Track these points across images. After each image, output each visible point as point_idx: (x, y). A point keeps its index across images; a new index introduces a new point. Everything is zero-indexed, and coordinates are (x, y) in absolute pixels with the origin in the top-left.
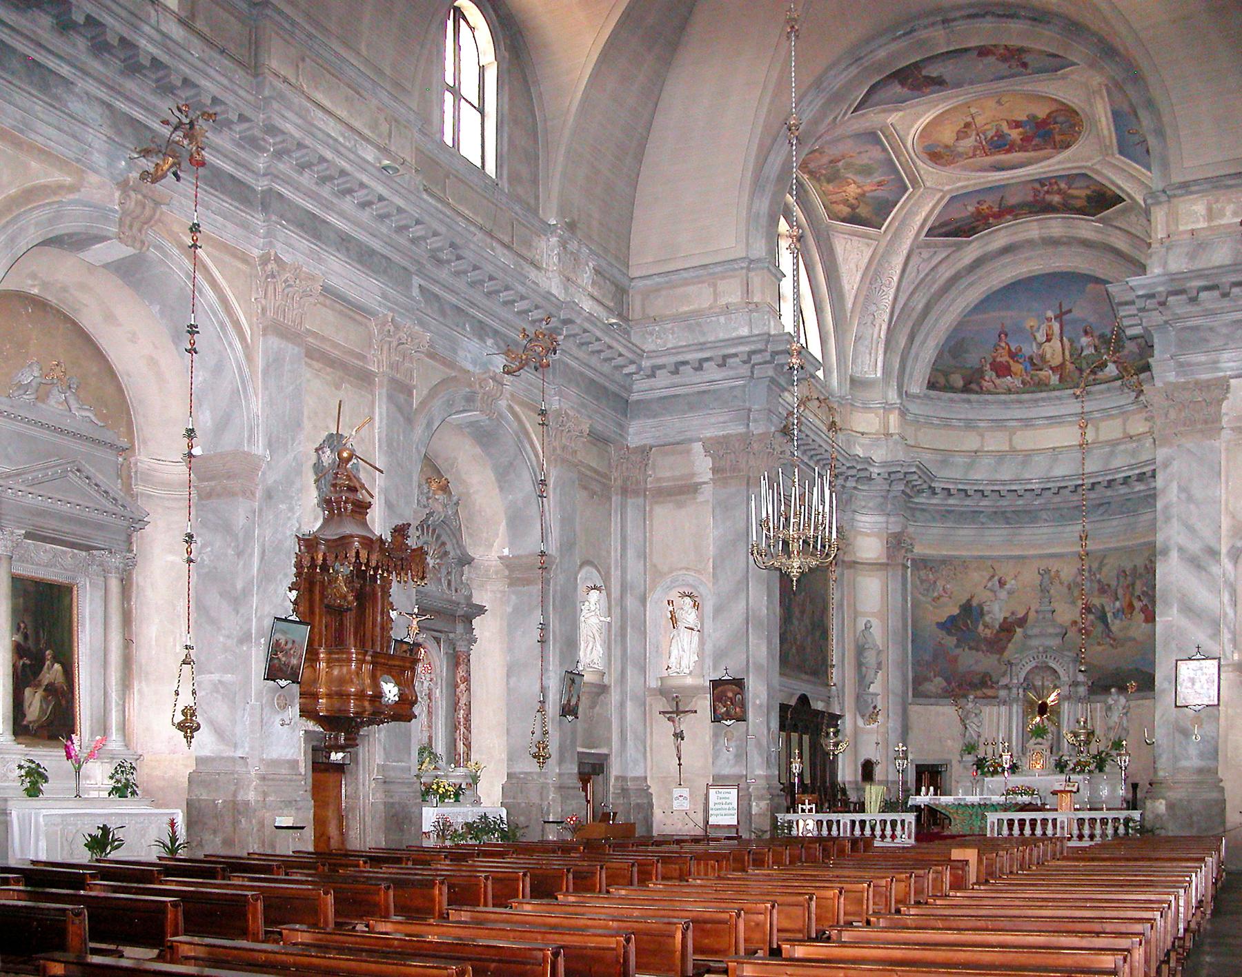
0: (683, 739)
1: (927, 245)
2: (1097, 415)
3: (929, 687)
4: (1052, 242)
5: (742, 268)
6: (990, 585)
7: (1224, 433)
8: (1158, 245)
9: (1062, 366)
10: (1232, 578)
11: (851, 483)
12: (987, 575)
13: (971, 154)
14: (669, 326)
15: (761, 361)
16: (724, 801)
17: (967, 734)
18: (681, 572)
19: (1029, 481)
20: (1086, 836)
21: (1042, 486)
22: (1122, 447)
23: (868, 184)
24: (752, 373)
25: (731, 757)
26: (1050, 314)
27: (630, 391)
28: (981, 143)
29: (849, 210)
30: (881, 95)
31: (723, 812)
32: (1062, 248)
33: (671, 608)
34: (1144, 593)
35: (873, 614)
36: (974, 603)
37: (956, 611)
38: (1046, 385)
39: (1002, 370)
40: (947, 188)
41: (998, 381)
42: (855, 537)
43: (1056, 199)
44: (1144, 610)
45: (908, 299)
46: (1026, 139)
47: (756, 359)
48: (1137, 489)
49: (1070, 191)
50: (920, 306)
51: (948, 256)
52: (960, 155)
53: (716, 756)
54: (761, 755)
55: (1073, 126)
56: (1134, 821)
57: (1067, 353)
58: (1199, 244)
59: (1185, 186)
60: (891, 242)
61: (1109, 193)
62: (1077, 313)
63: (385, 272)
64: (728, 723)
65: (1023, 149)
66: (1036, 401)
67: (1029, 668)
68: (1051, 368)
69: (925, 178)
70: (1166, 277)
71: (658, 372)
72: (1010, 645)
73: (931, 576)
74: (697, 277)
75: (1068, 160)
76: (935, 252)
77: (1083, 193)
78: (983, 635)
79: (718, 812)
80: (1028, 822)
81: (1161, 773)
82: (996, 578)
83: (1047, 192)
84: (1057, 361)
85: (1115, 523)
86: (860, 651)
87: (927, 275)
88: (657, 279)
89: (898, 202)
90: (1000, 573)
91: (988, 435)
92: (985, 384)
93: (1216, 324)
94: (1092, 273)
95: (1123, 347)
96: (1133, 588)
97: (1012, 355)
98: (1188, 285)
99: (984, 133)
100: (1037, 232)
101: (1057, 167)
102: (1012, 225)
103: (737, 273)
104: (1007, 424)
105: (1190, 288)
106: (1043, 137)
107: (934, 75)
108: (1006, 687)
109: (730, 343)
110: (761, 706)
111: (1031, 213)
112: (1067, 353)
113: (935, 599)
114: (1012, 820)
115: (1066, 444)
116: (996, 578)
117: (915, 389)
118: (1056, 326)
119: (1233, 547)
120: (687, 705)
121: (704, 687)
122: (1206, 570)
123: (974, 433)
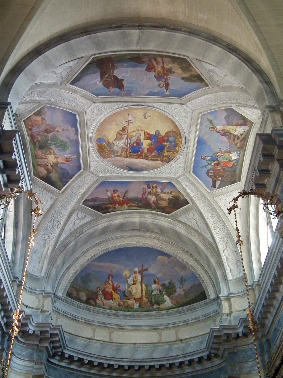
1: (82, 210)
9: (141, 299)
13: (119, 154)
19: (121, 360)
22: (176, 346)
26: (136, 269)
28: (127, 146)
29: (46, 172)
38: (132, 308)
39: (108, 296)
40: (101, 175)
41: (105, 302)
43: (153, 198)
48: (187, 371)
49: (162, 195)
52: (114, 152)
55: (176, 145)
61: (182, 198)
62: (151, 271)
65: (146, 158)
66: (126, 316)
68: (135, 299)
77: (166, 197)
84: (138, 296)
89: (73, 176)
91: (97, 330)
92: (98, 302)
94: (162, 250)
95: (175, 291)
97: (115, 289)
100: (138, 219)
107: (120, 77)
111: (139, 207)
117: (60, 294)
118: (139, 277)
123: (90, 328)
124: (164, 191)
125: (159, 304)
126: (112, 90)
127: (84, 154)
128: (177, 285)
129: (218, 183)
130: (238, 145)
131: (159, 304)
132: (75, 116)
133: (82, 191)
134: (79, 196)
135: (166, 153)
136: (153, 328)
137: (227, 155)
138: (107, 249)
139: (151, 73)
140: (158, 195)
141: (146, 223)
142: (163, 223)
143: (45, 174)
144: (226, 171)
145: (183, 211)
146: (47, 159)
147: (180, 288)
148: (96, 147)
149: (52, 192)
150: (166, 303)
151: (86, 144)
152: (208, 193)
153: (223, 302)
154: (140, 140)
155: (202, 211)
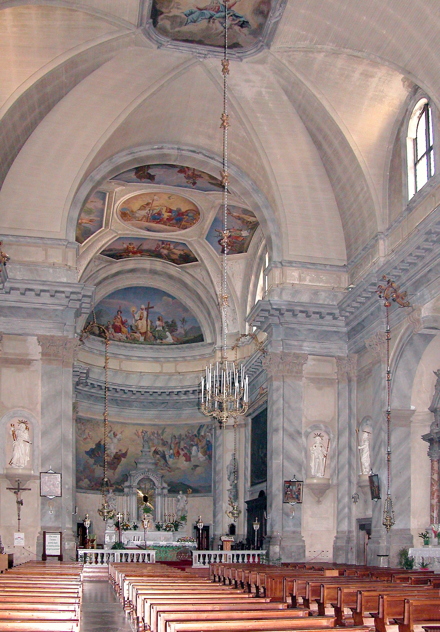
0: (22, 505)
1: (99, 259)
2: (162, 359)
4: (153, 272)
5: (64, 245)
6: (109, 435)
7: (304, 379)
8: (276, 287)
9: (145, 333)
15: (76, 299)
16: (53, 541)
19: (131, 386)
21: (137, 390)
22: (175, 377)
25: (52, 517)
26: (143, 307)
30: (125, 176)
31: (53, 548)
32: (156, 276)
33: (12, 429)
34: (185, 447)
36: (102, 443)
37: (94, 447)
38: (138, 341)
39: (118, 330)
40: (120, 232)
41: (115, 334)
43: (165, 252)
44: (185, 455)
47: (73, 297)
49: (174, 250)
51: (105, 267)
52: (135, 218)
53: (43, 515)
59: (290, 262)
62: (156, 309)
65: (165, 224)
68: (141, 333)
69: (112, 224)
70: (286, 303)
73: (83, 427)
74: (34, 243)
75: (182, 235)
76: (101, 263)
77: (178, 252)
79: (50, 548)
81: (275, 533)
82: (112, 432)
84: (144, 330)
85: (170, 412)
87: (94, 274)
88: (11, 238)
89: (95, 232)
90: (114, 430)
93: (301, 329)
97: (123, 323)
99: (153, 211)
100: (149, 266)
101: (175, 237)
102: (139, 259)
104: (118, 356)
106: (177, 220)
107: (152, 174)
109: (61, 284)
110: (68, 489)
113: (85, 439)
114: (97, 554)
115: (146, 371)
116: (112, 432)
118: (145, 313)
120: (23, 486)
122: (296, 441)
124: (176, 248)
125: (162, 340)
126: (143, 180)
127: (107, 217)
128: (179, 324)
130: (250, 227)
131: (162, 340)
132: (105, 194)
133: (100, 244)
134: (98, 248)
135: (183, 223)
136: (156, 360)
137: (238, 232)
138: (117, 288)
140: (171, 250)
141: (156, 270)
144: (236, 243)
145: (191, 265)
147: (181, 328)
150: (168, 339)
151: (111, 211)
152: (217, 257)
153: (217, 351)
154: (161, 212)
155: (210, 271)
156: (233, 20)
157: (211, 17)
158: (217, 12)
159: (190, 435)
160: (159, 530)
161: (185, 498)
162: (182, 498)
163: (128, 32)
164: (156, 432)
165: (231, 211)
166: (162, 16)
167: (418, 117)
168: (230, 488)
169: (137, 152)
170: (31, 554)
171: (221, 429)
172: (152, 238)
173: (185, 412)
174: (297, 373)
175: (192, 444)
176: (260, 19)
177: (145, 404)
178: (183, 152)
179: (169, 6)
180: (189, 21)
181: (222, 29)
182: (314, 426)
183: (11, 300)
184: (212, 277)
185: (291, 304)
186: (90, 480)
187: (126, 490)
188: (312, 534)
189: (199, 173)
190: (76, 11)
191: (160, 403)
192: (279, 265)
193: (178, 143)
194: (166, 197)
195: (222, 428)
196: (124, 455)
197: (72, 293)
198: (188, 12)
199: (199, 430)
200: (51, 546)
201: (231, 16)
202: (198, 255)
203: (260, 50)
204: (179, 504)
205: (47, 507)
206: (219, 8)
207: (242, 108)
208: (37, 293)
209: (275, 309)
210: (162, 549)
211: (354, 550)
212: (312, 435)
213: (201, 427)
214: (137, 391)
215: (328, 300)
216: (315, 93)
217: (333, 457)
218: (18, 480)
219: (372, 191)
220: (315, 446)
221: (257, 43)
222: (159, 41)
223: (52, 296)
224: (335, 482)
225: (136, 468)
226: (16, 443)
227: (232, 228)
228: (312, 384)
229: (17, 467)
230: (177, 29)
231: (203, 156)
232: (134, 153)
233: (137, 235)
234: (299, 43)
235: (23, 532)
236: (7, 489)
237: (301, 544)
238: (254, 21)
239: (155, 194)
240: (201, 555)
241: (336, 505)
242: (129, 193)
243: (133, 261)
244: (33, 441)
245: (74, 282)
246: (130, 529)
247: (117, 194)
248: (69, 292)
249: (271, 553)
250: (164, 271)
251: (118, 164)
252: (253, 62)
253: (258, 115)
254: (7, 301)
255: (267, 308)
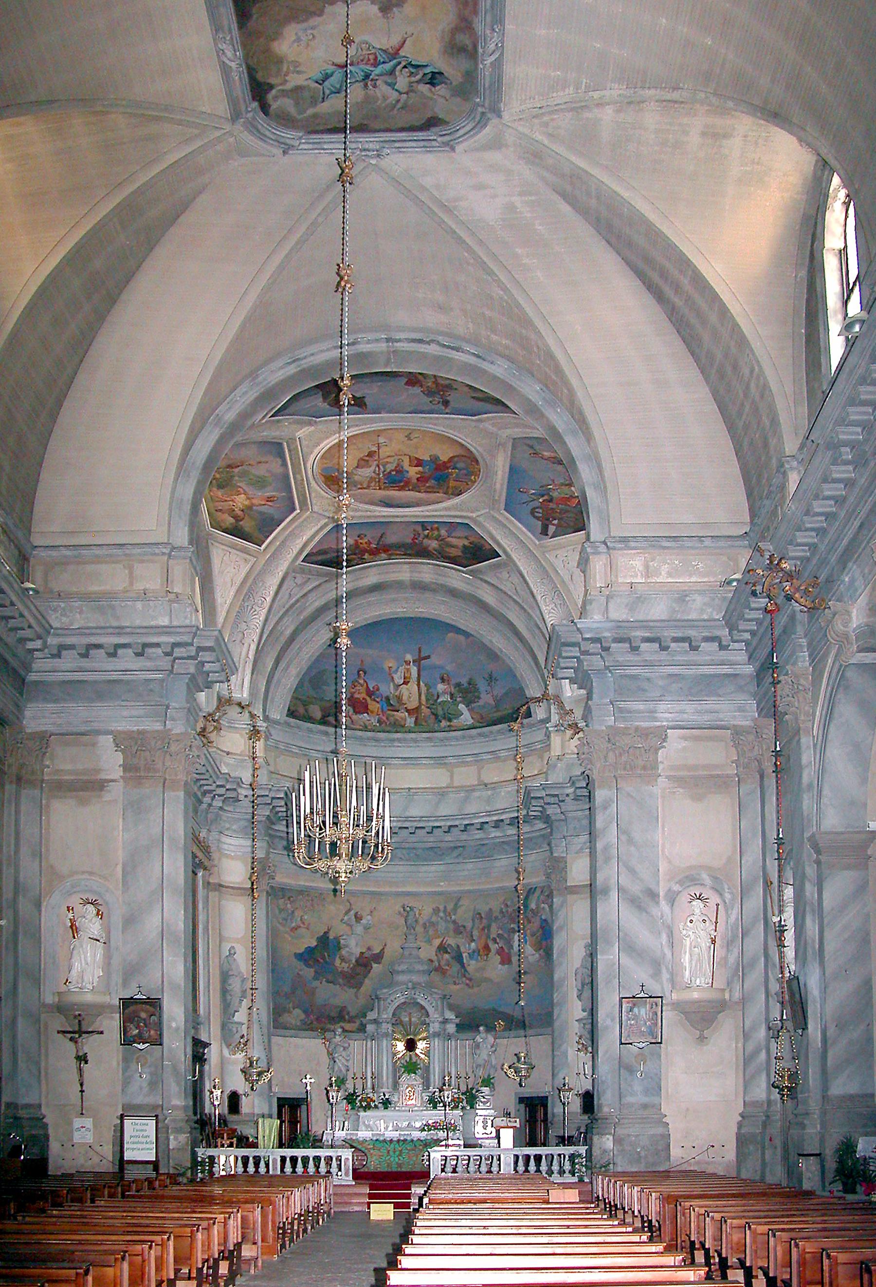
0: (86, 1062)
1: (302, 571)
2: (451, 760)
3: (286, 1018)
4: (419, 587)
5: (164, 554)
6: (346, 918)
7: (660, 779)
10: (669, 921)
11: (218, 803)
12: (343, 909)
14: (76, 604)
15: (185, 655)
16: (141, 1134)
17: (336, 1068)
18: (83, 877)
20: (567, 1172)
21: (400, 825)
22: (477, 794)
23: (258, 496)
24: (173, 667)
25: (145, 1084)
27: (28, 668)
28: (379, 474)
29: (232, 520)
30: (304, 404)
32: (428, 595)
33: (70, 915)
35: (237, 940)
38: (403, 726)
39: (358, 706)
41: (355, 717)
42: (220, 859)
43: (434, 544)
44: (500, 952)
45: (277, 623)
46: (422, 479)
47: (178, 652)
48: (493, 835)
49: (450, 539)
50: (288, 632)
51: (320, 585)
53: (126, 1082)
54: (178, 1083)
56: (580, 1155)
57: (423, 697)
58: (637, 598)
59: (624, 540)
60: (268, 562)
61: (488, 547)
62: (435, 660)
63: (669, 245)
64: (141, 1046)
65: (415, 489)
66: (393, 740)
67: (397, 1004)
68: (408, 711)
69: (314, 502)
71: (64, 653)
72: (367, 981)
73: (289, 905)
77: (461, 543)
78: (340, 970)
79: (135, 1146)
80: (300, 1159)
82: (353, 912)
83: (427, 536)
84: (413, 704)
86: (225, 977)
87: (297, 601)
90: (356, 908)
96: (489, 930)
97: (370, 693)
98: (633, 634)
99: (384, 466)
100: (408, 575)
101: (442, 513)
102: (384, 564)
103: (156, 558)
105: (635, 637)
106: (438, 479)
108: (375, 1021)
110: (177, 1029)
112: (423, 697)
115: (421, 786)
116: (353, 912)
118: (414, 670)
119: (669, 890)
121: (110, 1006)
122: (647, 912)
124: (453, 535)
125: (450, 720)
128: (482, 686)
129: (552, 529)
131: (450, 720)
132: (280, 444)
135: (452, 483)
136: (439, 761)
137: (566, 489)
139: (415, 388)
142: (454, 582)
143: (231, 524)
144: (567, 511)
145: (490, 566)
146: (232, 501)
148: (321, 480)
149: (244, 550)
151: (302, 476)
152: (535, 544)
156: (411, 74)
157: (367, 76)
158: (376, 64)
159: (510, 910)
160: (435, 1107)
161: (491, 1039)
162: (484, 1039)
163: (218, 134)
164: (441, 907)
165: (537, 447)
166: (274, 92)
167: (844, 203)
168: (581, 1017)
169: (305, 358)
170: (104, 1161)
171: (335, 895)
172: (398, 520)
173: (497, 864)
174: (644, 768)
175: (513, 928)
176: (465, 64)
177: (419, 852)
178: (398, 344)
179: (279, 70)
180: (327, 92)
181: (395, 95)
182: (687, 877)
183: (63, 669)
184: (531, 585)
185: (620, 627)
186: (305, 1012)
187: (370, 1028)
188: (688, 1109)
189: (447, 382)
190: (108, 113)
191: (451, 848)
192: (602, 549)
193: (387, 328)
194: (401, 437)
195: (338, 893)
196: (378, 958)
197: (175, 645)
198: (319, 76)
199: (527, 897)
200: (136, 1143)
201: (405, 67)
202: (499, 544)
203: (482, 123)
204: (478, 1052)
205: (133, 1066)
206: (376, 57)
207: (481, 243)
208: (109, 651)
209: (588, 639)
210: (392, 1145)
211: (778, 1142)
212: (684, 898)
213: (530, 892)
214: (400, 828)
215: (709, 610)
216: (618, 189)
217: (732, 941)
218: (80, 1015)
219: (769, 373)
220: (691, 921)
221: (473, 110)
222: (282, 140)
223: (139, 654)
224: (737, 995)
225: (391, 984)
226: (76, 942)
227: (551, 482)
228: (681, 790)
229: (77, 990)
230: (310, 111)
231: (438, 348)
232: (298, 359)
233: (369, 517)
234: (555, 95)
235: (90, 1117)
236: (58, 1032)
237: (660, 1130)
238: (452, 69)
239: (378, 433)
240: (288, 1159)
241: (740, 1045)
242: (327, 438)
243: (374, 569)
244: (108, 937)
245: (184, 624)
246: (376, 1107)
247: (304, 443)
248: (168, 643)
249: (596, 1152)
250: (440, 582)
251: (270, 385)
252: (477, 150)
253: (519, 251)
254: (59, 671)
255: (573, 640)
